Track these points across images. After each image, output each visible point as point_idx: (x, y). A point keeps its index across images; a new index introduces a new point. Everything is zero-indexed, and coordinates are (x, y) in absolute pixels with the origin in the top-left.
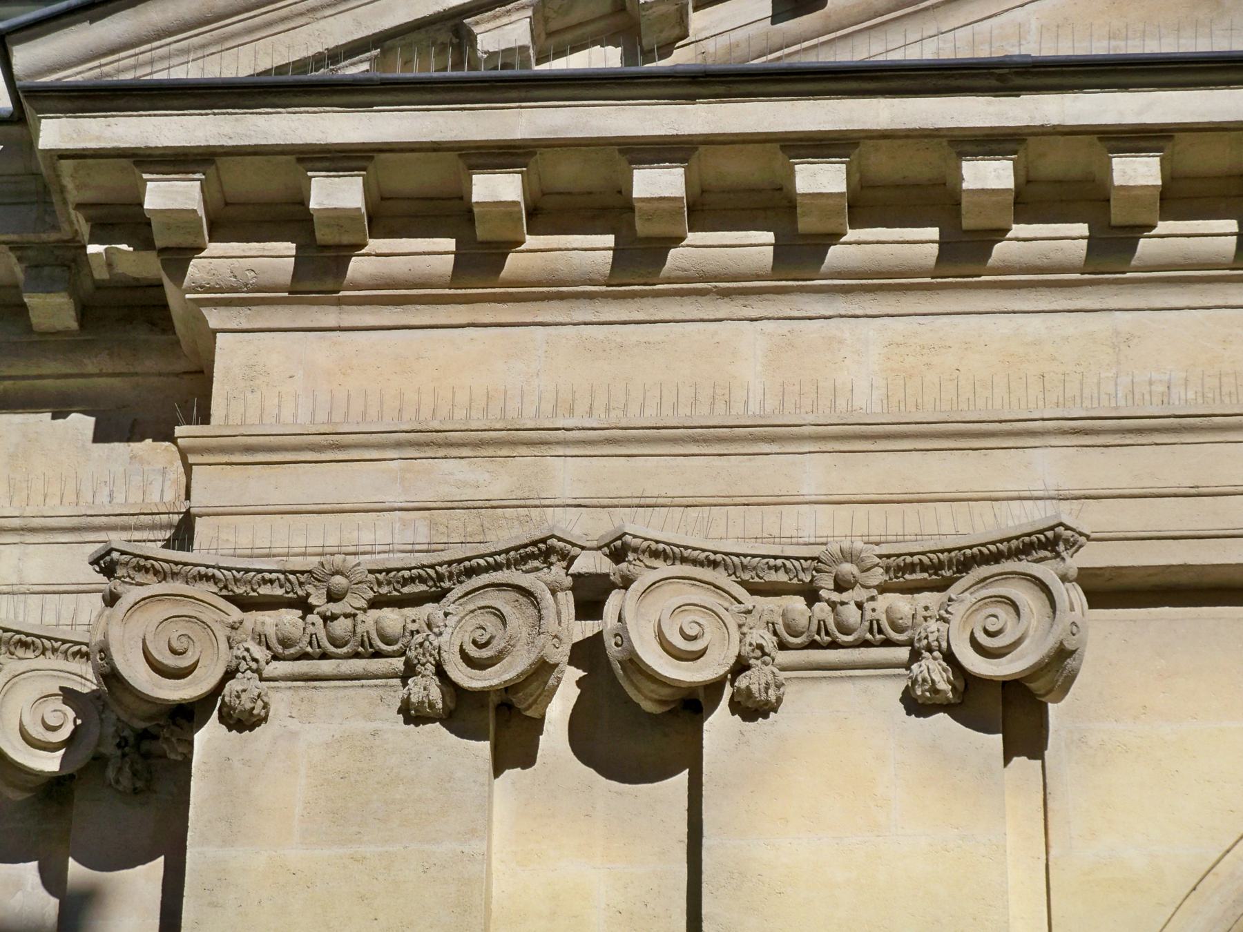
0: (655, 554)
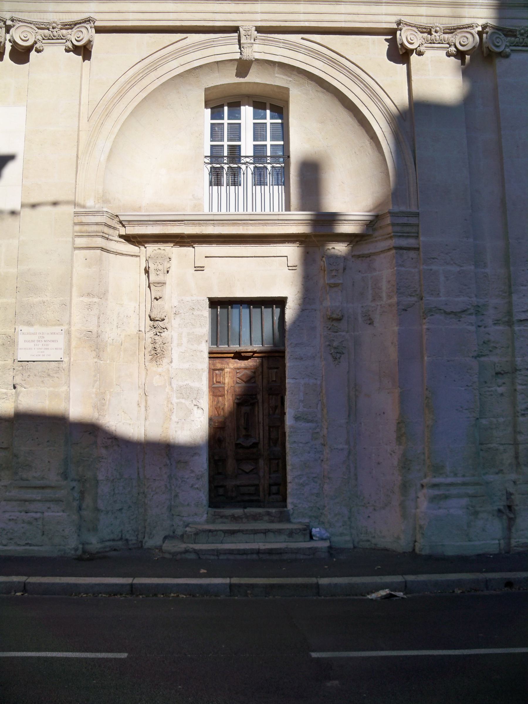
0: (19, 21)
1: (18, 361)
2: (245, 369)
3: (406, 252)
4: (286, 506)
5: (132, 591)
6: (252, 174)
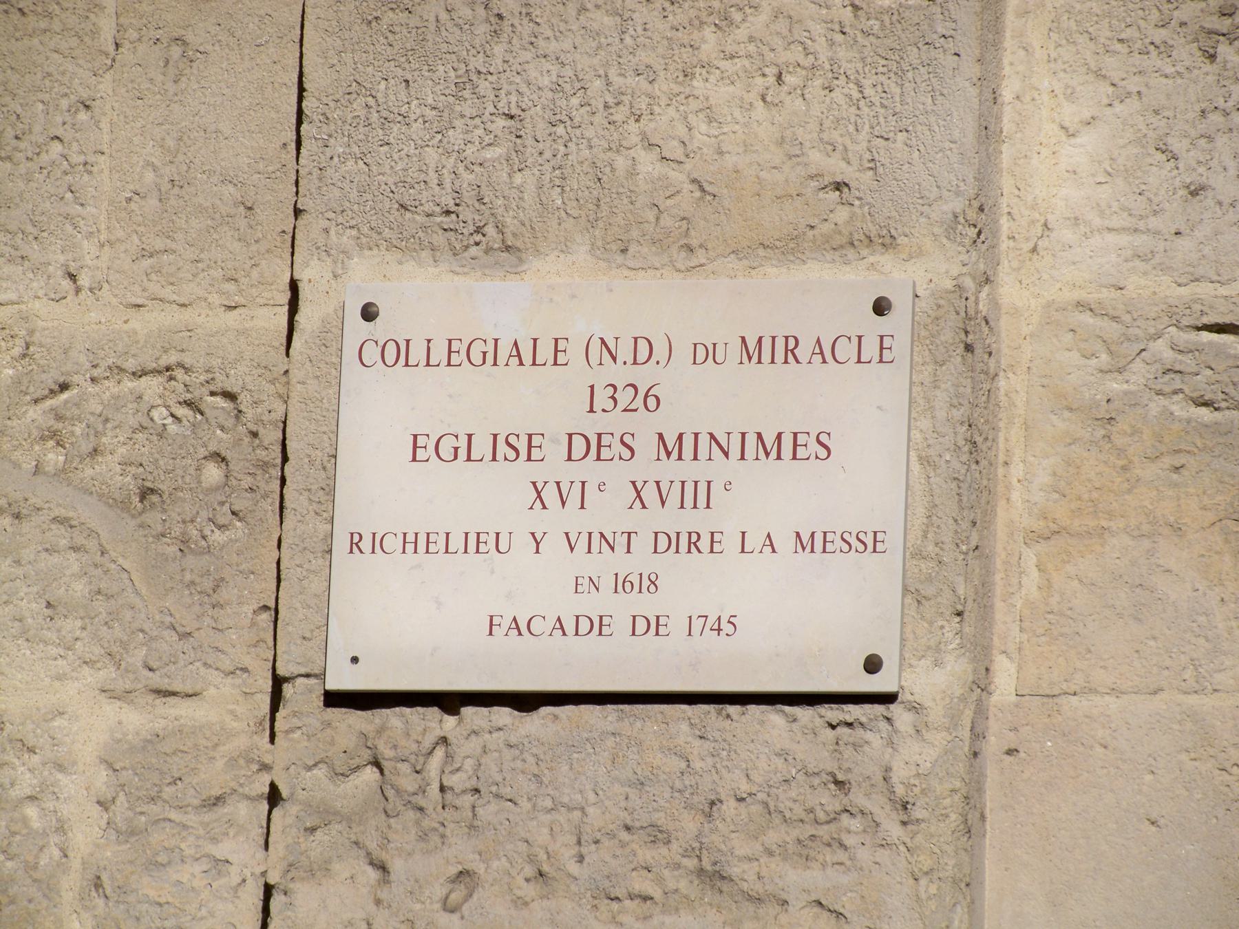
1: (335, 699)
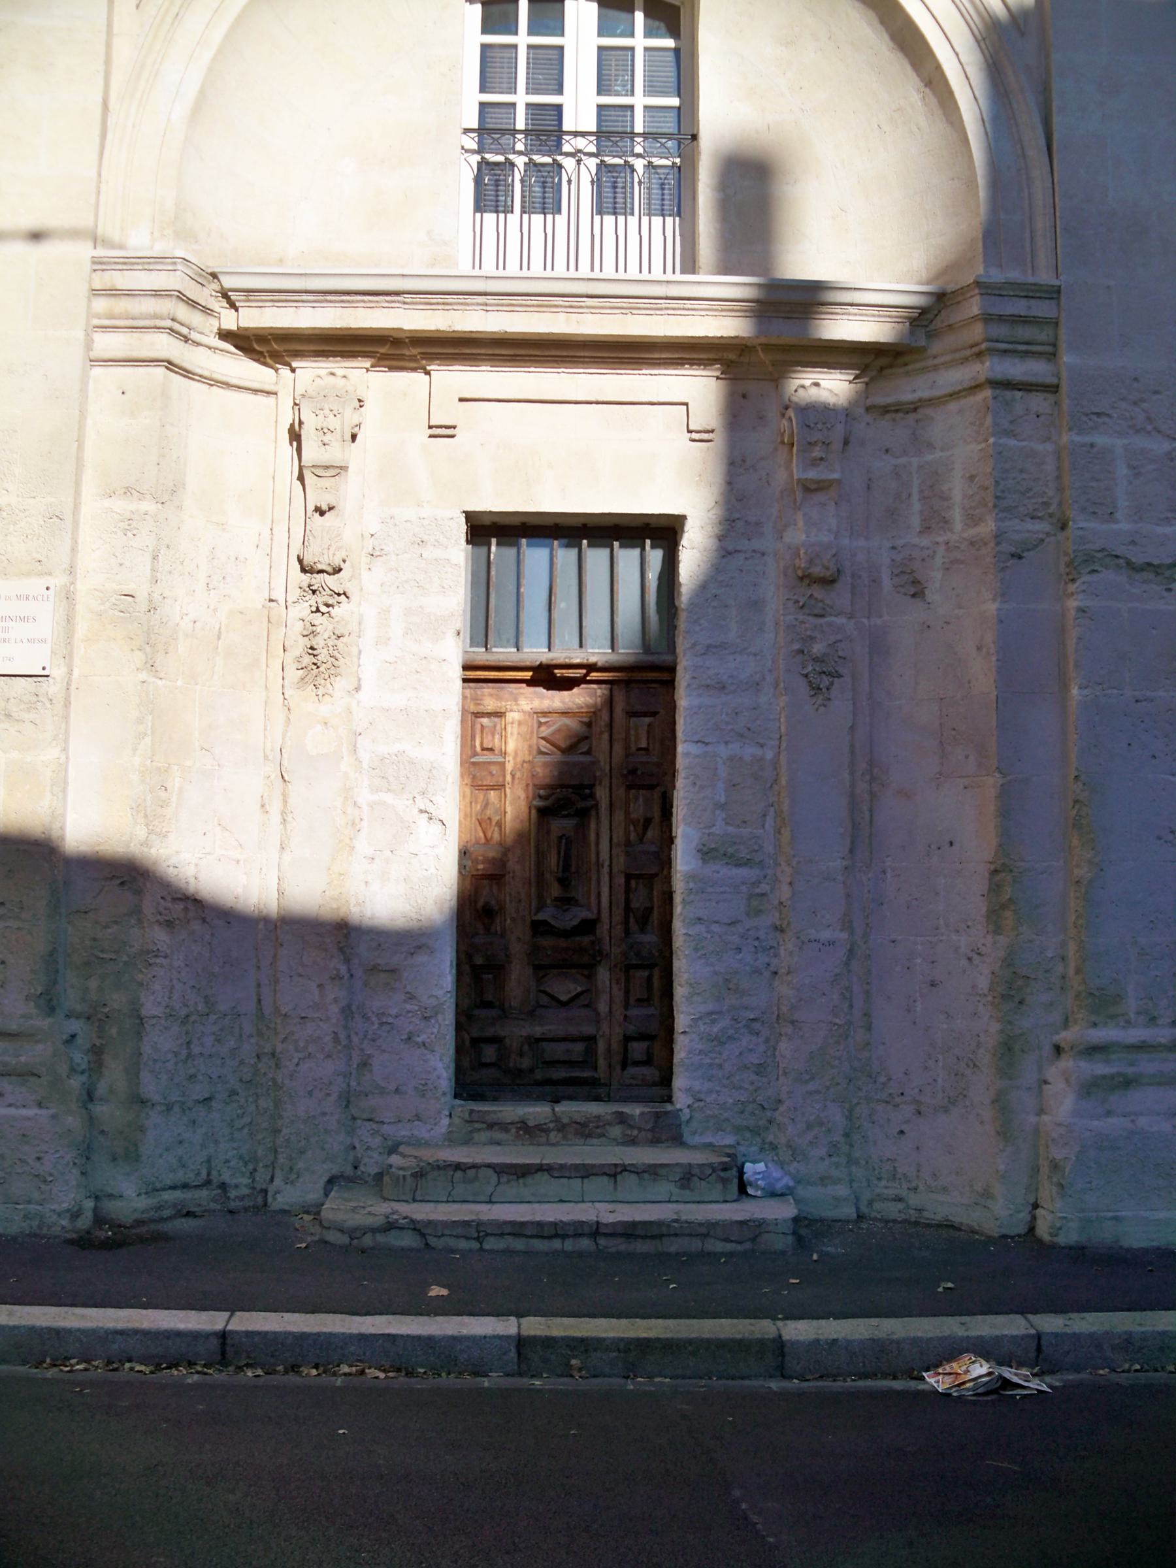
2: (564, 713)
3: (1021, 398)
4: (669, 1099)
5: (223, 1353)
6: (592, 182)
